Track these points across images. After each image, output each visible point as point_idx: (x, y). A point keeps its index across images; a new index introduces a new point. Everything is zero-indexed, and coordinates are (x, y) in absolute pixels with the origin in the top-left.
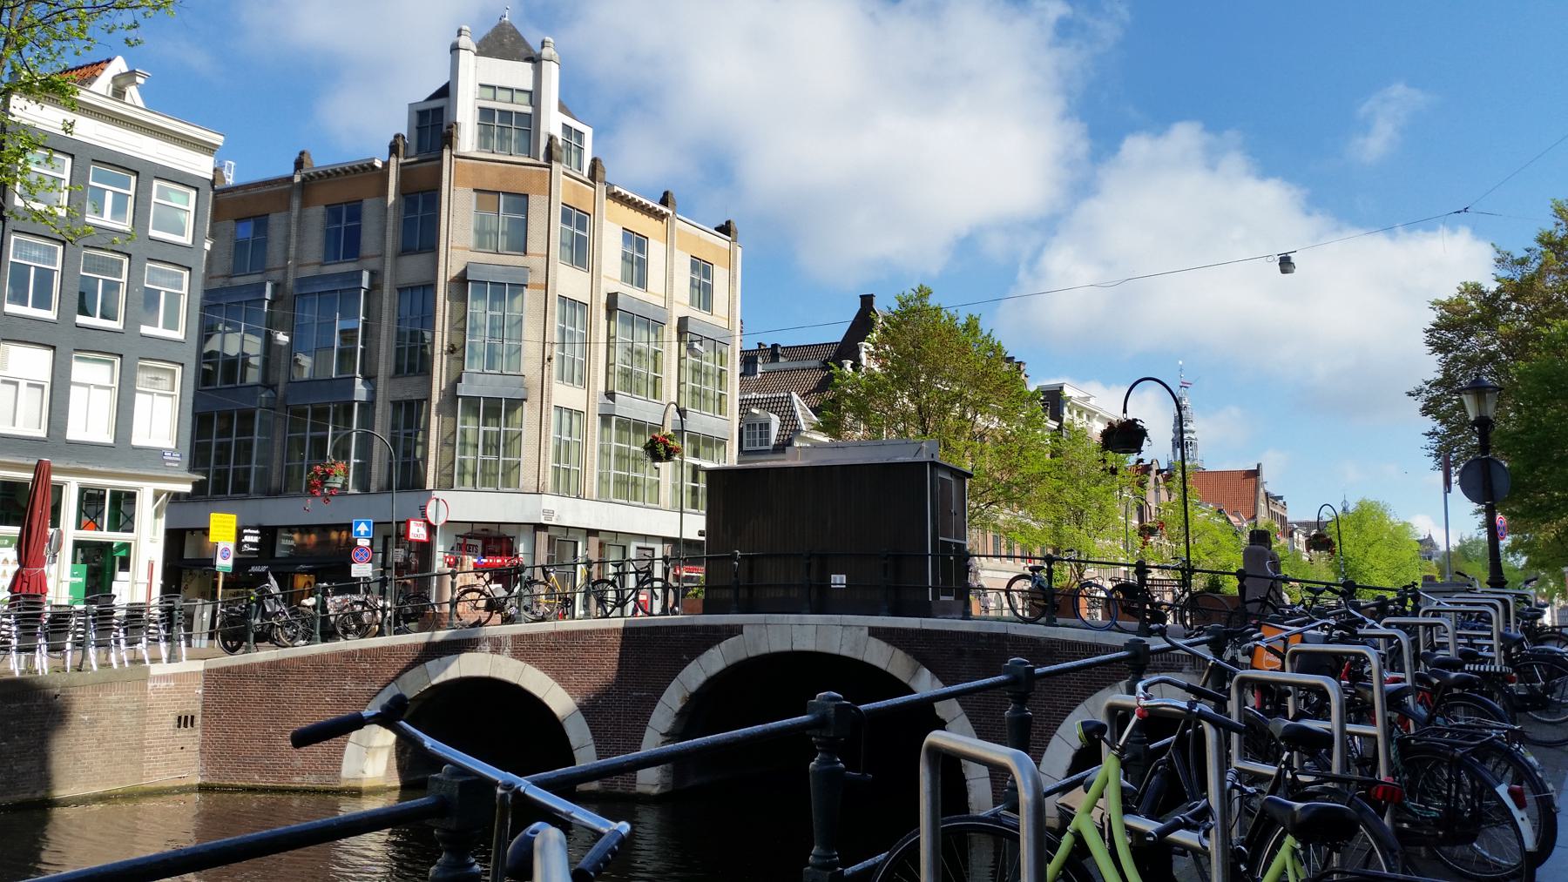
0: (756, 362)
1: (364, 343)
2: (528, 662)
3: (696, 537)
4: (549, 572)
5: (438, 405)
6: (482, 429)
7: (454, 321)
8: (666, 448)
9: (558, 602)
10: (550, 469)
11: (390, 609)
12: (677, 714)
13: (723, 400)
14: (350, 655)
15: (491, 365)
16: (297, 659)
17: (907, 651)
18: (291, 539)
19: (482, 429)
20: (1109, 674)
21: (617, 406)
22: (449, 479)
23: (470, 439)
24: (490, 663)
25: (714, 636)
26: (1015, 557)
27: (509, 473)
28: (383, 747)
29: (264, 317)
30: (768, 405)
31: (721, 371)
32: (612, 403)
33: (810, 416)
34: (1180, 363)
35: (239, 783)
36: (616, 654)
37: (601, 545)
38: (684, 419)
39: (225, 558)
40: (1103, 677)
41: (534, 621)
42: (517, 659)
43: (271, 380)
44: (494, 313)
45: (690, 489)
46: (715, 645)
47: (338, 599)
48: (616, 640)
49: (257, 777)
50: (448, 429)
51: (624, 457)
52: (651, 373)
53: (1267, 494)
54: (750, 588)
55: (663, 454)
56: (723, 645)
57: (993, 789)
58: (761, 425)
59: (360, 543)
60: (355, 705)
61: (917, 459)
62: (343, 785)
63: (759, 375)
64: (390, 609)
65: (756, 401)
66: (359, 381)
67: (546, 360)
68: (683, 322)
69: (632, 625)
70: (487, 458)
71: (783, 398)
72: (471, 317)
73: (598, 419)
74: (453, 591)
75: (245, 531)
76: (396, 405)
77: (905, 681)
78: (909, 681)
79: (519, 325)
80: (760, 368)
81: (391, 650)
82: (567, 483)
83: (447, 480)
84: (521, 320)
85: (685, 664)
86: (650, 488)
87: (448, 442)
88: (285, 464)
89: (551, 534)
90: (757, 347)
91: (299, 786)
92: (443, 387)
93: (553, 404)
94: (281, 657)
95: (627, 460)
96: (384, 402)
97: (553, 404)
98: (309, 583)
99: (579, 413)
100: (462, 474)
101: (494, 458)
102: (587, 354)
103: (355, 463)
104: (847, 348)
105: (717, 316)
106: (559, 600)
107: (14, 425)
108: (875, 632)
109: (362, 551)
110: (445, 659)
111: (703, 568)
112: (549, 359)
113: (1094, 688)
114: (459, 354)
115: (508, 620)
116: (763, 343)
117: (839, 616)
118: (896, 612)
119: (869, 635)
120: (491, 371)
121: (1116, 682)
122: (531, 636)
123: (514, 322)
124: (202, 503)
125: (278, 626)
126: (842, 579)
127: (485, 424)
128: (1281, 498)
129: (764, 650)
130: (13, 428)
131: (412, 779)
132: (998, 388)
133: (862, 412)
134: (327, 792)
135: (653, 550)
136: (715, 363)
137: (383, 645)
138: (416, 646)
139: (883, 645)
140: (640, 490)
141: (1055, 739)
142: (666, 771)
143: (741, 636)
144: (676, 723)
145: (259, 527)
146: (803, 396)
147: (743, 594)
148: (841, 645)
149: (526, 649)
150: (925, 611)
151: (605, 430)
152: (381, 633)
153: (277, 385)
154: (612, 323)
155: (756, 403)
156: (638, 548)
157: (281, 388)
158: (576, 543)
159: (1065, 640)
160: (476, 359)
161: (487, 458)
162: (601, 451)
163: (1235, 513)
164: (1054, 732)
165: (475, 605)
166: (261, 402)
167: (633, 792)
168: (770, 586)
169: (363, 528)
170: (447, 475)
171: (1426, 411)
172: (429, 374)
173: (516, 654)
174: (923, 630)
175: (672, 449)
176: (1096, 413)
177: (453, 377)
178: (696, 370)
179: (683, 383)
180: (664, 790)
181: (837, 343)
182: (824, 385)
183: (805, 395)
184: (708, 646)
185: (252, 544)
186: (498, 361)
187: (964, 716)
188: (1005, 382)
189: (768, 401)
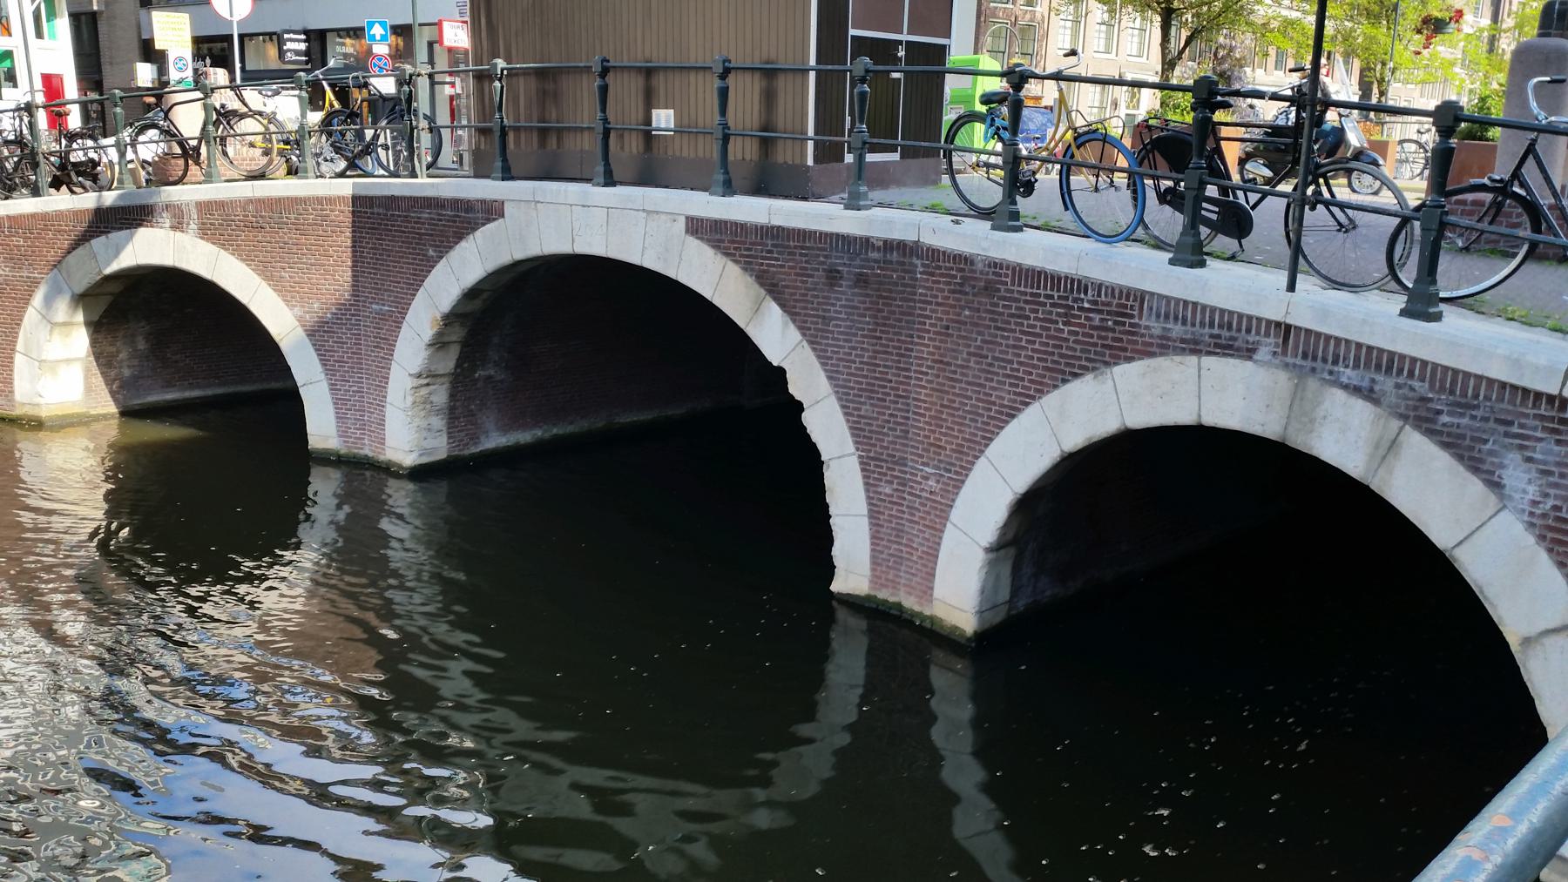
2: (223, 246)
17: (747, 267)
20: (1095, 345)
24: (172, 245)
36: (346, 239)
39: (180, 70)
40: (1082, 351)
42: (208, 240)
48: (344, 216)
56: (478, 233)
57: (873, 537)
60: (14, 298)
62: (18, 412)
75: (286, 36)
77: (741, 324)
85: (430, 264)
108: (698, 227)
109: (380, 60)
110: (116, 236)
113: (1064, 372)
119: (687, 231)
121: (1107, 364)
131: (139, 402)
138: (77, 213)
139: (708, 252)
141: (981, 464)
143: (501, 220)
145: (306, 32)
148: (644, 248)
152: (413, 175)
164: (982, 452)
169: (377, 31)
180: (425, 460)
184: (460, 237)
185: (297, 53)
187: (833, 399)
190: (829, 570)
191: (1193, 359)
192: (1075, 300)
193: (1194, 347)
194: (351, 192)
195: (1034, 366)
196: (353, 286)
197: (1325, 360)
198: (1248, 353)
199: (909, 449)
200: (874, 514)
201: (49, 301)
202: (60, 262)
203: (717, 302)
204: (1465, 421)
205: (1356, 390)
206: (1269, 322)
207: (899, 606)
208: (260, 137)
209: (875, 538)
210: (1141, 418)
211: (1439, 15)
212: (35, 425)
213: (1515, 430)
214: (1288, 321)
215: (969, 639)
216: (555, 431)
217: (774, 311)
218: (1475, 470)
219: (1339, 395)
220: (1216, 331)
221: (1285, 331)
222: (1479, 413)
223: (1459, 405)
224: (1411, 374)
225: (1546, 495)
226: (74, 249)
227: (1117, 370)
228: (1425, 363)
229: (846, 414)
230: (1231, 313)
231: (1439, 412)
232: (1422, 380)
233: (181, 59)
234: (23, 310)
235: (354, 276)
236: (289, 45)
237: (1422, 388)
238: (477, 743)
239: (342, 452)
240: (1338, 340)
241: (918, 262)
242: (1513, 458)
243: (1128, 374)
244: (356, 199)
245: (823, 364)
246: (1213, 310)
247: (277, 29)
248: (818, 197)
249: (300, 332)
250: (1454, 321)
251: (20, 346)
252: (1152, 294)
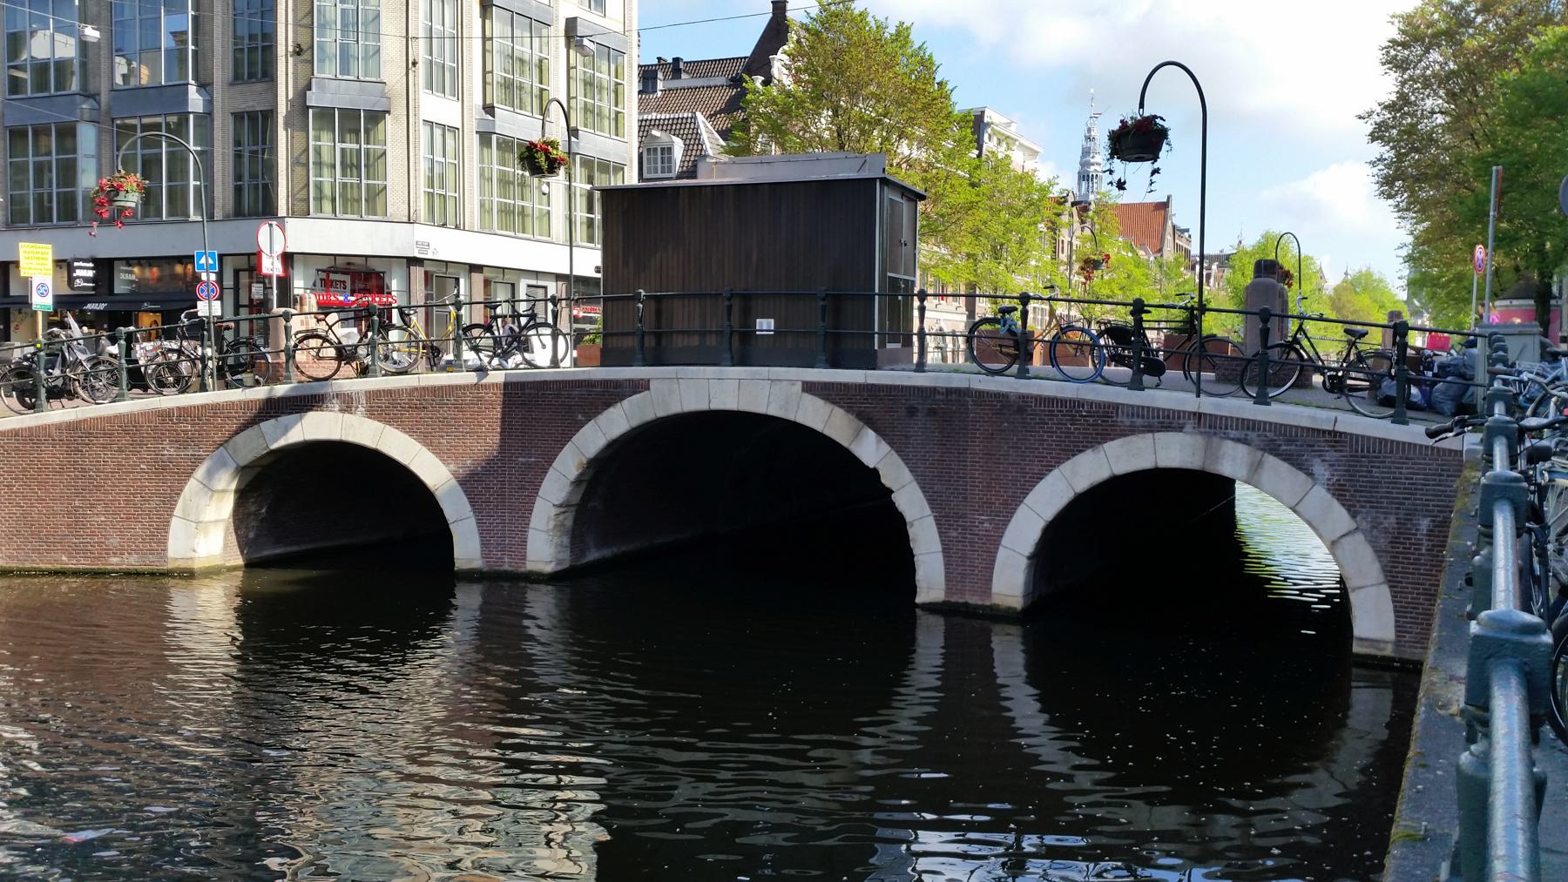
0: (655, 78)
1: (195, 43)
2: (388, 423)
3: (592, 274)
4: (409, 315)
5: (286, 117)
6: (339, 146)
7: (299, 16)
8: (547, 158)
9: (421, 351)
10: (422, 194)
11: (211, 358)
12: (573, 483)
13: (620, 90)
14: (165, 415)
15: (345, 69)
16: (102, 419)
17: (849, 410)
18: (131, 272)
19: (339, 146)
21: (497, 123)
22: (304, 204)
23: (326, 158)
25: (612, 393)
26: (947, 295)
27: (374, 199)
28: (217, 521)
29: (77, 10)
30: (671, 127)
31: (617, 84)
32: (490, 118)
33: (717, 140)
34: (1092, 91)
35: (43, 566)
36: (497, 413)
37: (487, 283)
38: (573, 139)
39: (42, 295)
41: (394, 374)
43: (92, 89)
44: (345, 6)
45: (585, 220)
47: (149, 346)
48: (497, 398)
49: (64, 558)
50: (299, 147)
51: (509, 183)
52: (536, 84)
53: (1174, 227)
54: (658, 336)
55: (545, 166)
56: (626, 402)
57: (946, 564)
58: (663, 149)
59: (204, 277)
60: (177, 473)
61: (865, 174)
62: (171, 566)
63: (659, 93)
64: (211, 358)
65: (657, 122)
66: (192, 89)
67: (410, 65)
68: (571, 24)
69: (514, 380)
70: (348, 180)
71: (687, 118)
72: (319, 11)
73: (476, 138)
74: (288, 337)
75: (76, 264)
76: (238, 117)
77: (845, 444)
79: (376, 21)
80: (660, 85)
81: (215, 408)
82: (443, 212)
83: (300, 206)
84: (378, 16)
85: (581, 425)
86: (541, 218)
87: (300, 161)
88: (9, 160)
89: (428, 269)
90: (656, 62)
91: (117, 567)
92: (290, 96)
93: (422, 118)
94: (81, 416)
95: (511, 186)
96: (223, 113)
97: (422, 118)
98: (156, 322)
99: (454, 129)
100: (320, 199)
101: (355, 180)
102: (458, 55)
103: (195, 186)
104: (759, 62)
105: (611, 19)
106: (424, 348)
108: (809, 388)
110: (284, 419)
111: (601, 308)
112: (414, 64)
114: (306, 56)
115: (364, 372)
116: (663, 57)
117: (767, 368)
118: (835, 364)
119: (803, 390)
120: (346, 77)
121: (1100, 443)
122: (389, 392)
123: (371, 19)
124: (24, 232)
125: (75, 380)
126: (769, 324)
127: (343, 141)
128: (1187, 230)
129: (675, 408)
131: (258, 555)
132: (926, 107)
133: (777, 132)
134: (153, 574)
135: (545, 288)
136: (609, 75)
137: (208, 402)
139: (820, 402)
140: (528, 221)
142: (561, 546)
144: (571, 493)
145: (94, 260)
146: (710, 117)
147: (650, 342)
149: (384, 407)
150: (870, 362)
151: (485, 149)
152: (203, 388)
153: (99, 94)
154: (487, 21)
155: (657, 124)
156: (529, 286)
157: (104, 98)
158: (457, 280)
159: (1040, 396)
160: (327, 61)
161: (348, 180)
162: (482, 175)
163: (1142, 246)
164: (1021, 502)
165: (318, 354)
166: (82, 113)
167: (523, 570)
168: (683, 332)
170: (302, 200)
171: (1374, 137)
172: (272, 80)
173: (372, 413)
174: (868, 385)
175: (555, 160)
176: (1016, 140)
177: (302, 83)
178: (589, 84)
179: (573, 98)
180: (559, 568)
181: (745, 58)
182: (733, 106)
183: (711, 116)
184: (608, 405)
185: (86, 279)
186: (353, 66)
187: (915, 483)
188: (935, 99)
189: (670, 122)
190: (913, 590)
191: (1150, 435)
192: (1077, 412)
193: (1150, 429)
194: (503, 380)
195: (1053, 449)
196: (500, 446)
197: (1221, 428)
198: (1180, 429)
200: (946, 551)
201: (210, 474)
202: (226, 441)
203: (827, 432)
204: (1293, 447)
205: (1238, 440)
206: (1190, 413)
207: (966, 604)
209: (947, 565)
210: (1121, 468)
211: (1095, 258)
212: (188, 575)
213: (1316, 448)
214: (1200, 411)
215: (1019, 613)
216: (623, 549)
217: (870, 435)
218: (1300, 469)
219: (1230, 443)
220: (1161, 420)
221: (1199, 416)
222: (1298, 443)
223: (1288, 440)
224: (1265, 430)
225: (1333, 475)
226: (242, 431)
227: (1105, 445)
228: (1271, 423)
229: (924, 492)
230: (1169, 410)
231: (1280, 445)
232: (1270, 431)
233: (43, 285)
234: (185, 482)
235: (501, 439)
236: (79, 273)
237: (1270, 435)
239: (485, 570)
240: (1227, 418)
241: (969, 399)
242: (1317, 461)
243: (1112, 447)
244: (506, 385)
245: (906, 464)
246: (1159, 409)
247: (68, 256)
248: (880, 369)
249: (454, 482)
250: (1275, 406)
251: (178, 511)
252: (1123, 405)
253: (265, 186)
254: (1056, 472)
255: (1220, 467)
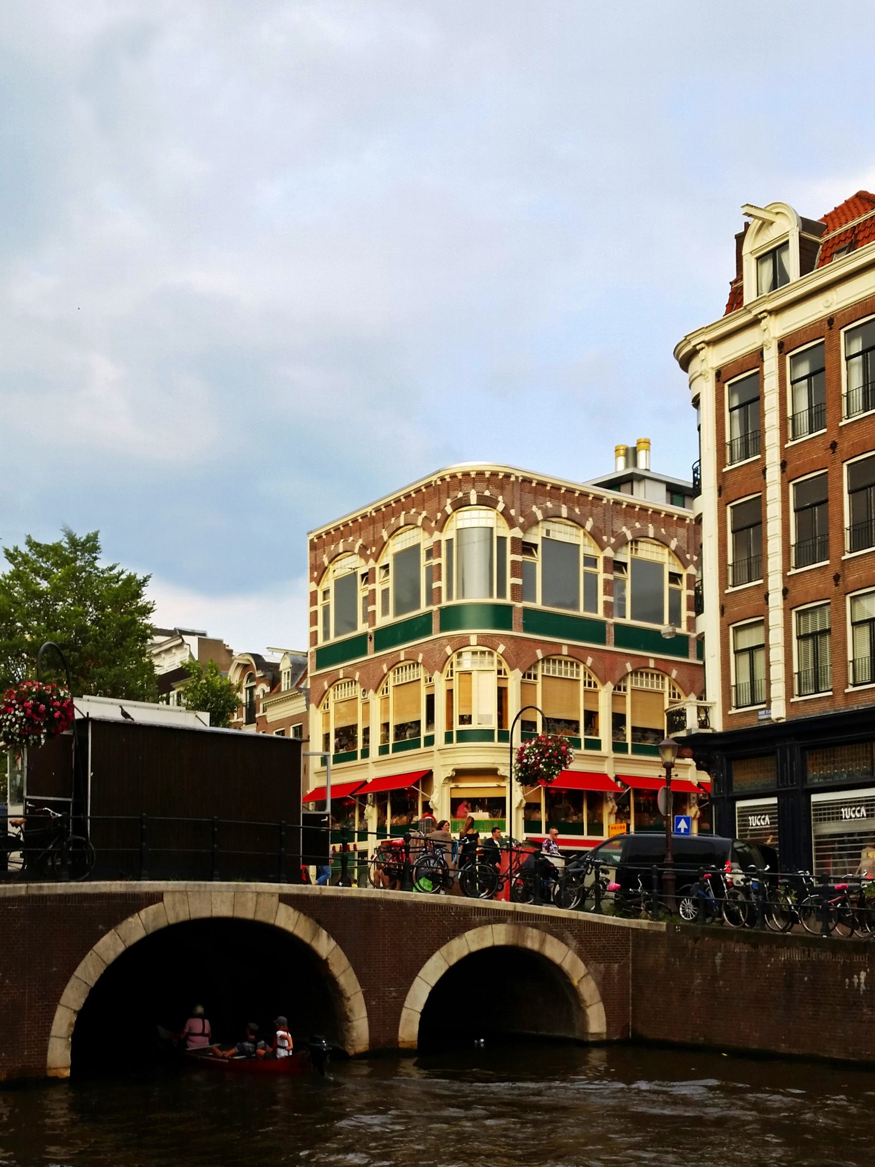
46: (135, 913)
78: (311, 941)
107: (632, 494)
108: (285, 899)
130: (631, 496)
139: (291, 910)
141: (417, 979)
143: (161, 904)
193: (489, 923)
199: (837, 846)
208: (509, 835)
210: (474, 948)
219: (530, 929)
227: (466, 934)
238: (676, 1158)
243: (470, 935)
253: (857, 242)
254: (437, 954)
255: (525, 944)
